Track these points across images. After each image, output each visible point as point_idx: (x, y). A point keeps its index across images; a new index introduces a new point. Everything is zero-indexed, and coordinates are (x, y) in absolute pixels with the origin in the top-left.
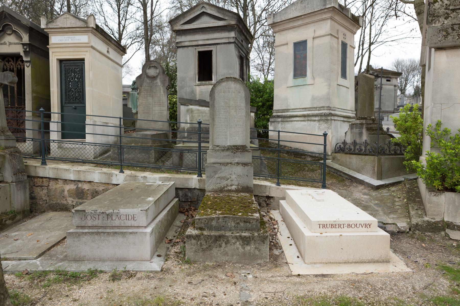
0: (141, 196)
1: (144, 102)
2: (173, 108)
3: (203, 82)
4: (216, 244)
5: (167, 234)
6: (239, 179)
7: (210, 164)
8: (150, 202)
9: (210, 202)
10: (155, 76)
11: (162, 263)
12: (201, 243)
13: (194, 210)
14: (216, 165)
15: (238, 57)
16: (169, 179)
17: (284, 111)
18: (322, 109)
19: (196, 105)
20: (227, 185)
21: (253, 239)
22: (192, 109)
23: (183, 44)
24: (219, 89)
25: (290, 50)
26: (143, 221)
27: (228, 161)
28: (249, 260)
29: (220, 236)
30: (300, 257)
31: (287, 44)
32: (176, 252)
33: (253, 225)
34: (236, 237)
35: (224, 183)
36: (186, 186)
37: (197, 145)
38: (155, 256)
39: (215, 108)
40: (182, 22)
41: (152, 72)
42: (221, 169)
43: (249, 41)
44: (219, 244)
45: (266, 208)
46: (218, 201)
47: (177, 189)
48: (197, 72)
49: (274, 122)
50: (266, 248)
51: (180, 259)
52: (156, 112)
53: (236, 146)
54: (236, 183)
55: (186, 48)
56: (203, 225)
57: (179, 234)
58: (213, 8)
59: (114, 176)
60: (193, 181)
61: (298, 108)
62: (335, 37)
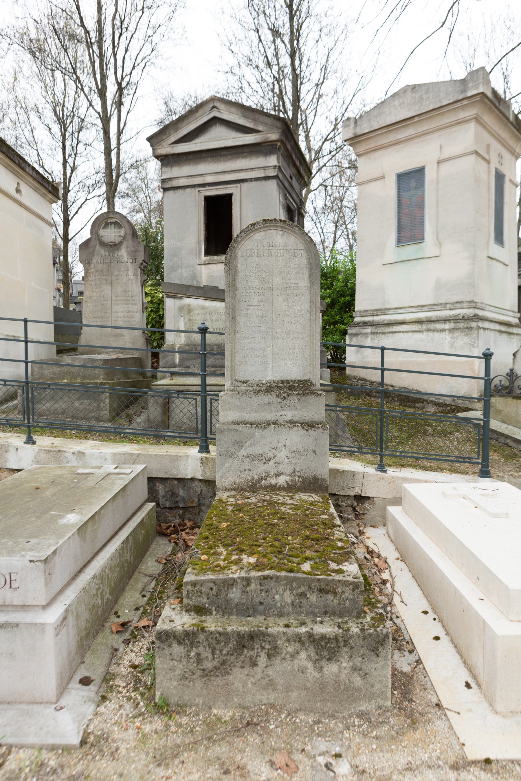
0: (50, 510)
1: (95, 294)
2: (157, 311)
3: (216, 257)
4: (242, 658)
5: (121, 601)
6: (294, 461)
7: (228, 423)
8: (67, 526)
9: (224, 525)
10: (117, 242)
11: (90, 709)
12: (198, 655)
13: (192, 528)
15: (284, 207)
16: (134, 459)
17: (376, 312)
18: (458, 306)
19: (198, 296)
20: (268, 475)
21: (346, 643)
22: (189, 305)
23: (175, 183)
25: (389, 189)
26: (35, 589)
27: (270, 416)
28: (334, 703)
29: (252, 636)
30: (473, 684)
31: (383, 177)
32: (134, 667)
33: (345, 600)
34: (299, 639)
35: (259, 470)
36: (173, 473)
37: (197, 381)
38: (74, 684)
39: (238, 292)
40: (173, 139)
41: (110, 234)
42: (252, 436)
43: (303, 178)
44: (251, 658)
45: (355, 524)
46: (246, 518)
47: (151, 480)
48: (202, 237)
49: (356, 335)
50: (383, 667)
51: (142, 695)
52: (120, 315)
53: (288, 382)
54: (289, 470)
55: (180, 191)
56: (205, 600)
57: (151, 599)
58: (233, 110)
59: (12, 450)
60: (187, 461)
62: (484, 158)
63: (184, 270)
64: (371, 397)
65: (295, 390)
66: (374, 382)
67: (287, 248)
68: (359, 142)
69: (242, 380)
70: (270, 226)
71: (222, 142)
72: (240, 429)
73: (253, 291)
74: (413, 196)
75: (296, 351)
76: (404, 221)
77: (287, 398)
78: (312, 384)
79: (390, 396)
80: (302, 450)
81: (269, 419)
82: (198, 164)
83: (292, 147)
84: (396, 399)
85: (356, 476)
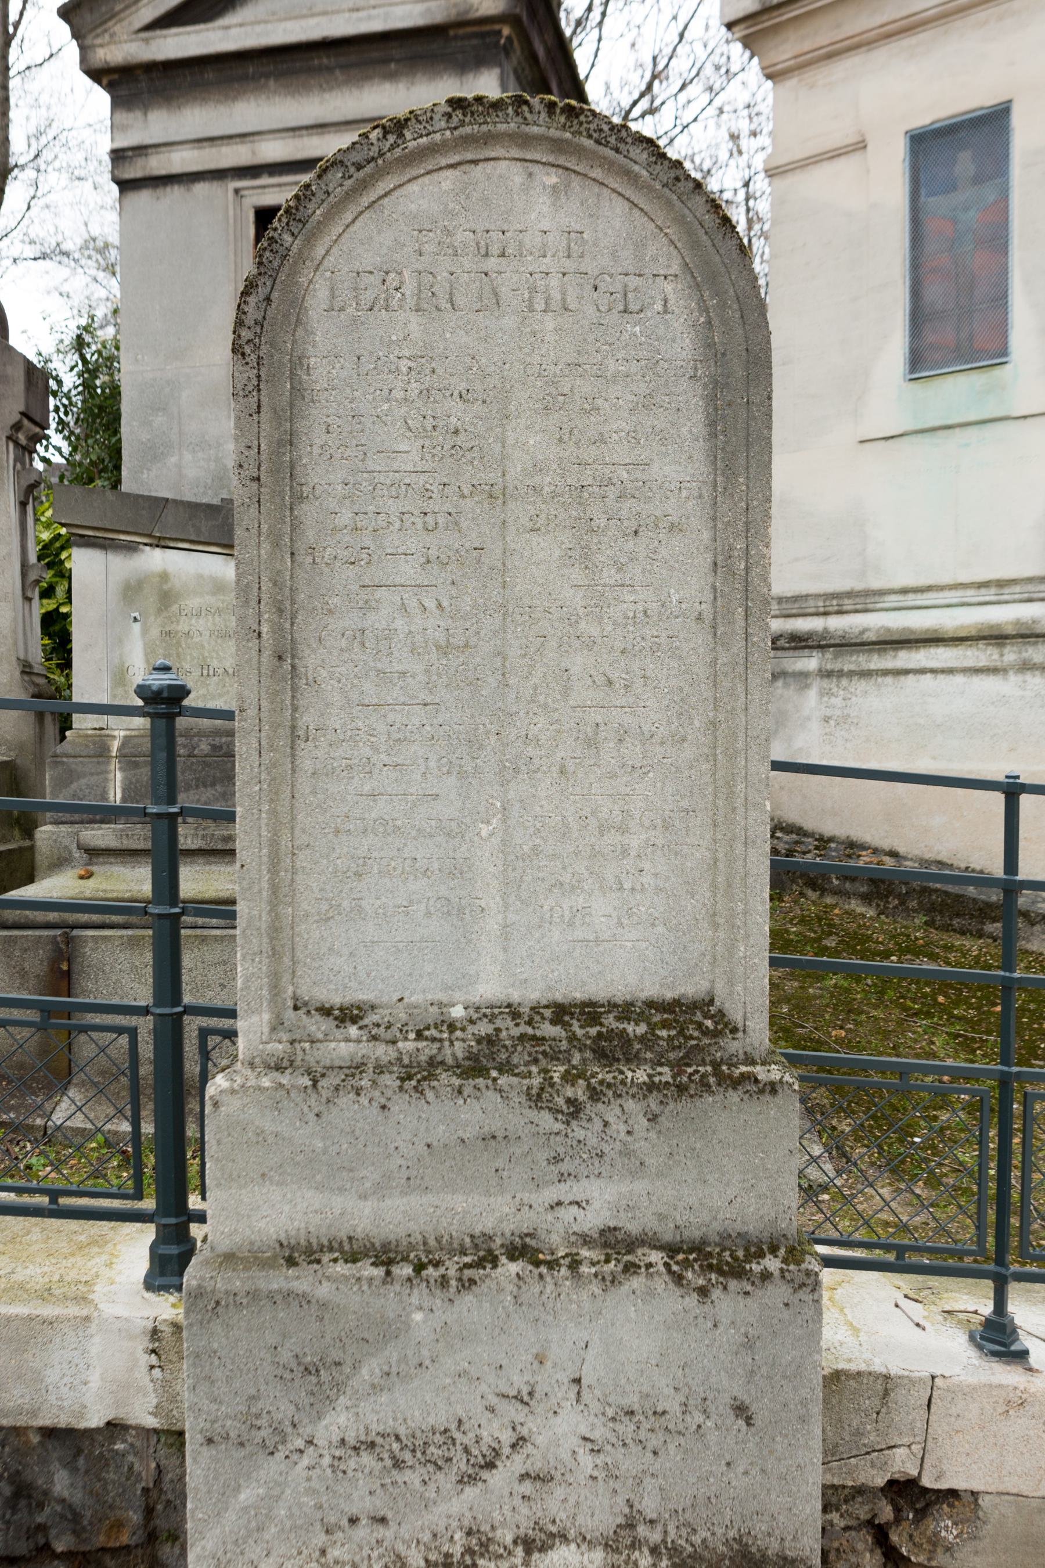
6: (630, 1462)
14: (331, 1283)
17: (837, 602)
22: (164, 576)
23: (157, 165)
24: (368, 259)
25: (883, 184)
31: (861, 146)
39: (308, 512)
42: (391, 1331)
53: (590, 1011)
55: (175, 193)
61: (946, 579)
63: (188, 457)
64: (823, 891)
65: (633, 1059)
66: (831, 840)
67: (589, 266)
68: (776, 28)
69: (337, 1000)
70: (488, 139)
71: (313, 21)
72: (324, 1291)
73: (393, 507)
74: (966, 209)
75: (635, 842)
76: (934, 292)
77: (590, 1109)
78: (725, 1026)
79: (890, 893)
80: (673, 1406)
81: (486, 1224)
82: (235, 99)
83: (548, 51)
84: (913, 904)
85: (898, 1395)
